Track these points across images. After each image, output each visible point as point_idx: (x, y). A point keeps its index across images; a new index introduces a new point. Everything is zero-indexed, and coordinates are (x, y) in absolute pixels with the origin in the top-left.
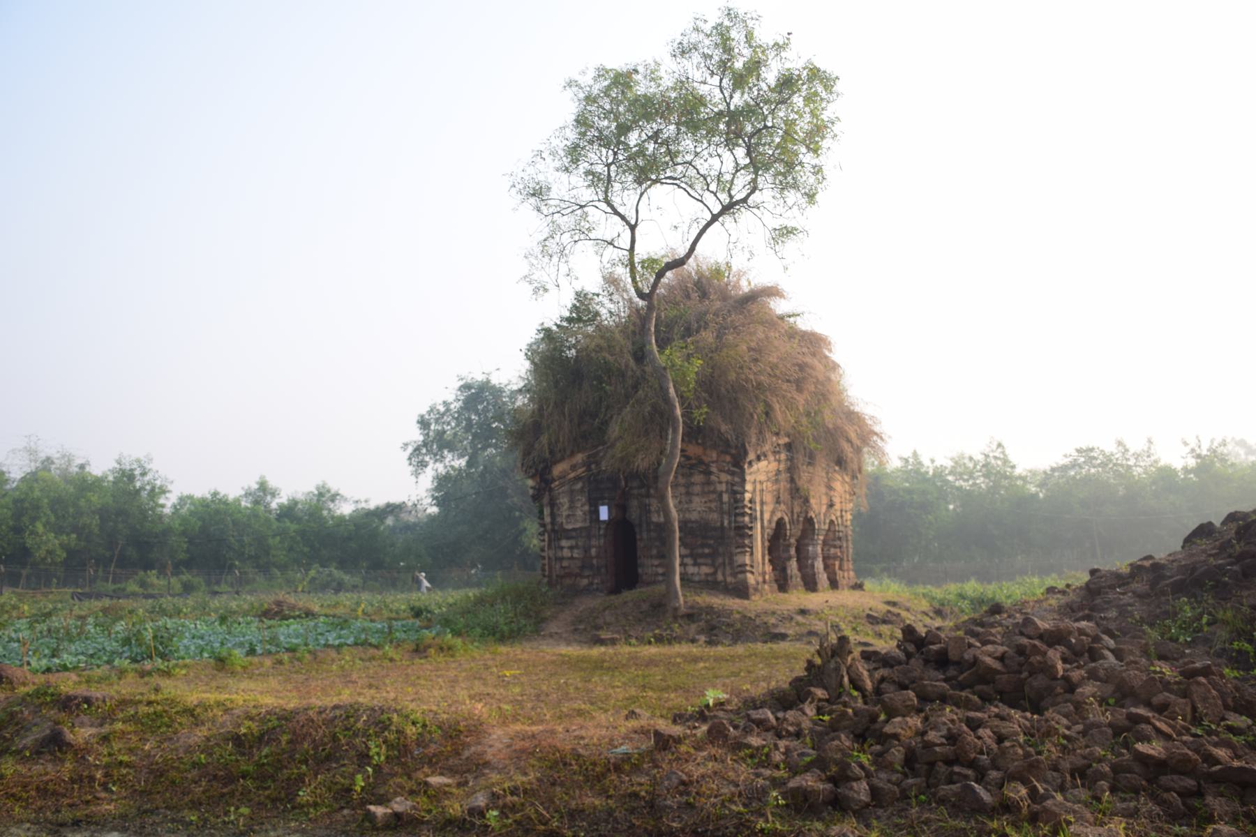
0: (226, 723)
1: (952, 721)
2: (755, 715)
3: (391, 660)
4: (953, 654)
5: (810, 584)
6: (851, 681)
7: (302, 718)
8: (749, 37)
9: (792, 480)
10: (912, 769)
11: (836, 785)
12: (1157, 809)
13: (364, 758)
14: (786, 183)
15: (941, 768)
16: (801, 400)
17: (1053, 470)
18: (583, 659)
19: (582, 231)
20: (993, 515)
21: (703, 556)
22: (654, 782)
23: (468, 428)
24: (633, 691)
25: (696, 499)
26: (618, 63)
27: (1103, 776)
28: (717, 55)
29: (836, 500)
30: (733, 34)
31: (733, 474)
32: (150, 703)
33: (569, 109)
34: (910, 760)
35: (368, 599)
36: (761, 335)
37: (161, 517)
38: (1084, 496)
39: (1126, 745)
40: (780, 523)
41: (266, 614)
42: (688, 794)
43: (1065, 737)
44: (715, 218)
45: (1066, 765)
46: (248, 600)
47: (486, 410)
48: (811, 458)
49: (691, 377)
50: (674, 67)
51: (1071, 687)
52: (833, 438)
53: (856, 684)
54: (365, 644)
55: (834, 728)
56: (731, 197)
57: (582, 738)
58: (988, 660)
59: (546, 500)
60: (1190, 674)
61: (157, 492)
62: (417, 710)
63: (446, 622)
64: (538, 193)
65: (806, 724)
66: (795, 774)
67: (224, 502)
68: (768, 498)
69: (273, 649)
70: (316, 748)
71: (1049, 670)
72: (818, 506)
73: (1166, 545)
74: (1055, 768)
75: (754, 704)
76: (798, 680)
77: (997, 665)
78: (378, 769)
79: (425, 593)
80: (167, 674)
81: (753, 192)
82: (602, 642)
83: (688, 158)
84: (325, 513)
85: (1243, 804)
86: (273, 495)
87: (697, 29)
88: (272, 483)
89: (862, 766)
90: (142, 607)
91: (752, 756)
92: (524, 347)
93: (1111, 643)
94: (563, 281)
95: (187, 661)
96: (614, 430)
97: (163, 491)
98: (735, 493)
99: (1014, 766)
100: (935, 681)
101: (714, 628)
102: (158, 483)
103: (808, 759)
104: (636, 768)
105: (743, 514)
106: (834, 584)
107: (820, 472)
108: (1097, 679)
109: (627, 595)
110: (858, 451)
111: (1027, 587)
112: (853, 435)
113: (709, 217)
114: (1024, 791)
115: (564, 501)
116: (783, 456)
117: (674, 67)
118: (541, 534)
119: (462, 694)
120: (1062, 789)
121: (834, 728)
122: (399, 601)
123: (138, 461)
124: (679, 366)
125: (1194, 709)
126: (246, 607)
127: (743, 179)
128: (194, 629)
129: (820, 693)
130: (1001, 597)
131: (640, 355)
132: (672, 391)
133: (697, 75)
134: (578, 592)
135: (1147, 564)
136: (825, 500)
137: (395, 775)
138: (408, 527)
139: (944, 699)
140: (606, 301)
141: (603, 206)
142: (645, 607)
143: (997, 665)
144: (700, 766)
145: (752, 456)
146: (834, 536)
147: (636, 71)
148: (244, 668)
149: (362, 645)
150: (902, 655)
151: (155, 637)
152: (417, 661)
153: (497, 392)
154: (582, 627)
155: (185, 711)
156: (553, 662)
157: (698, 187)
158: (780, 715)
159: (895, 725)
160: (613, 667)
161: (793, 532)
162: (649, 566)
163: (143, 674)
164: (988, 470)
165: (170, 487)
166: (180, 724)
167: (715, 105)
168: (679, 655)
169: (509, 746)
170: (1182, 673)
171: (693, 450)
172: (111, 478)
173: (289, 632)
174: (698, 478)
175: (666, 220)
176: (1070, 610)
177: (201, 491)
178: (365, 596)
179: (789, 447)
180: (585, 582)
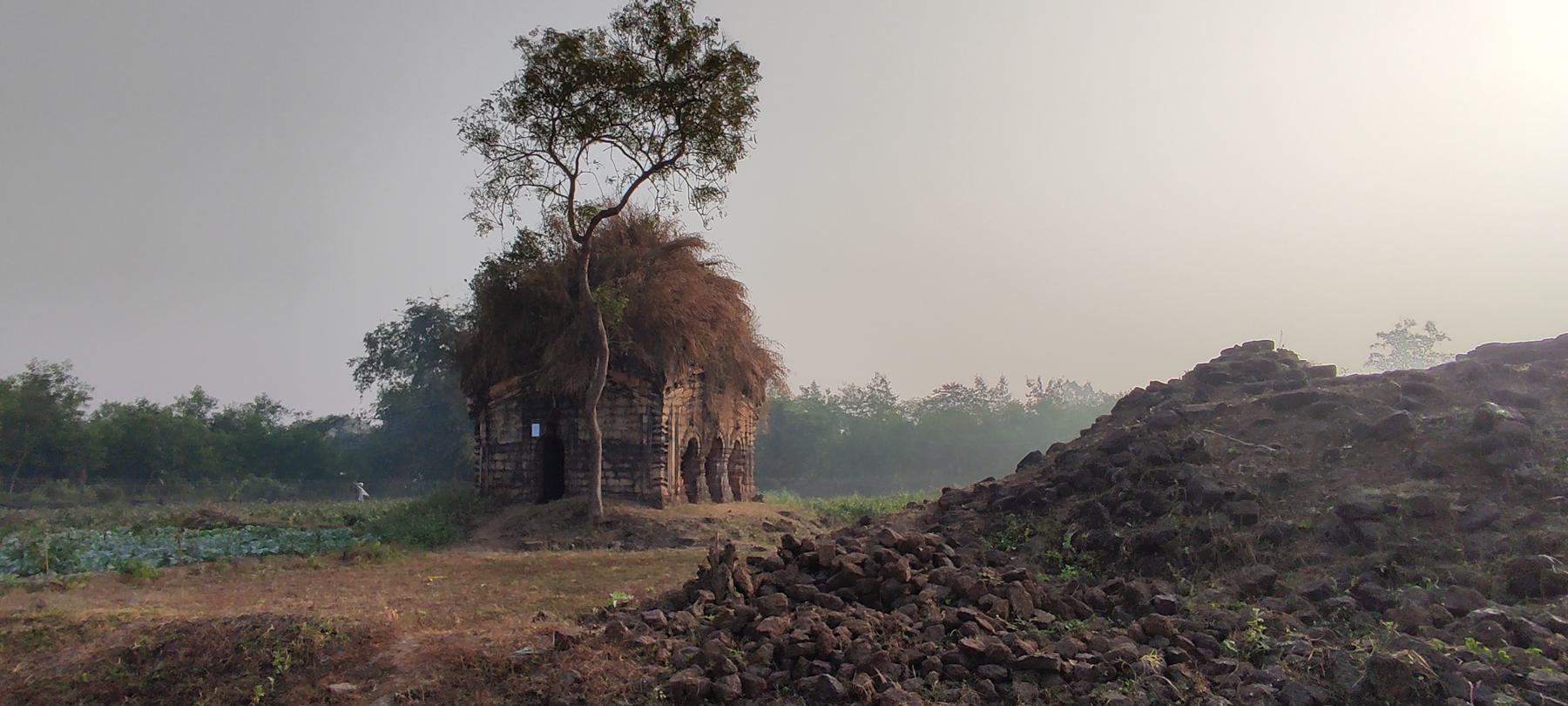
0: (118, 639)
1: (816, 620)
2: (649, 615)
3: (316, 568)
4: (823, 560)
5: (717, 497)
6: (736, 584)
7: (204, 631)
8: (684, 18)
9: (704, 405)
10: (779, 663)
11: (713, 680)
12: (975, 694)
13: (267, 667)
14: (707, 152)
15: (803, 661)
16: (714, 336)
17: (926, 402)
18: (506, 564)
19: (527, 175)
20: (867, 435)
21: (622, 470)
22: (552, 680)
23: (415, 349)
24: (548, 593)
25: (620, 420)
26: (565, 28)
27: (934, 667)
28: (655, 32)
29: (742, 424)
30: (670, 14)
31: (653, 399)
32: (29, 621)
33: (516, 65)
34: (778, 654)
35: (299, 509)
36: (683, 280)
37: (77, 424)
38: (955, 413)
39: (956, 640)
40: (692, 443)
41: (189, 523)
42: (581, 691)
43: (907, 633)
44: (645, 175)
45: (906, 657)
46: (174, 508)
47: (433, 332)
48: (722, 388)
49: (619, 313)
50: (616, 38)
51: (917, 589)
52: (739, 367)
53: (739, 587)
54: (290, 552)
55: (717, 626)
56: (661, 158)
57: (489, 640)
58: (851, 566)
59: (482, 416)
60: (1009, 578)
61: (74, 399)
62: (327, 616)
63: (377, 530)
64: (487, 139)
65: (693, 623)
66: (679, 669)
67: (154, 411)
68: (682, 420)
69: (190, 559)
70: (216, 658)
71: (899, 574)
72: (726, 429)
73: (1003, 470)
74: (897, 661)
75: (651, 606)
76: (691, 582)
77: (858, 570)
78: (280, 678)
79: (363, 501)
80: (63, 588)
81: (679, 155)
82: (527, 548)
83: (625, 120)
84: (264, 424)
85: (1041, 687)
86: (209, 405)
87: (638, 6)
88: (209, 393)
89: (736, 662)
90: (42, 518)
91: (642, 654)
92: (470, 278)
93: (952, 552)
94: (505, 220)
95: (88, 574)
96: (548, 357)
97: (82, 398)
98: (654, 415)
99: (863, 659)
100: (807, 584)
101: (629, 534)
102: (77, 390)
103: (690, 655)
104: (536, 667)
105: (660, 434)
106: (737, 496)
107: (729, 400)
108: (939, 583)
109: (552, 505)
110: (762, 382)
111: (899, 499)
112: (757, 369)
113: (640, 173)
114: (869, 682)
115: (499, 419)
116: (697, 385)
117: (616, 38)
118: (477, 448)
119: (381, 600)
120: (901, 679)
121: (717, 626)
122: (334, 509)
123: (55, 367)
124: (609, 304)
125: (1011, 608)
126: (168, 516)
127: (670, 146)
128: (101, 542)
129: (708, 595)
130: (877, 509)
131: (575, 291)
132: (601, 324)
133: (636, 47)
134: (506, 502)
135: (987, 484)
136: (732, 423)
137: (298, 683)
138: (352, 439)
139: (812, 600)
140: (547, 241)
141: (548, 156)
142: (568, 515)
143: (858, 570)
144: (595, 664)
145: (669, 384)
146: (738, 455)
147: (582, 38)
148: (154, 579)
149: (287, 553)
150: (781, 562)
151: (52, 550)
152: (343, 568)
153: (445, 316)
154: (509, 533)
155: (70, 628)
156: (478, 567)
157: (634, 147)
158: (671, 615)
159: (767, 624)
160: (520, 570)
161: (703, 451)
162: (574, 478)
163: (32, 588)
164: (873, 400)
165: (90, 394)
166: (63, 642)
167: (652, 76)
168: (597, 560)
169: (417, 651)
170: (1004, 578)
171: (619, 377)
172: (19, 383)
173: (208, 543)
174: (622, 401)
175: (602, 172)
176: (924, 523)
177: (128, 398)
178: (302, 504)
179: (702, 377)
180: (515, 492)
